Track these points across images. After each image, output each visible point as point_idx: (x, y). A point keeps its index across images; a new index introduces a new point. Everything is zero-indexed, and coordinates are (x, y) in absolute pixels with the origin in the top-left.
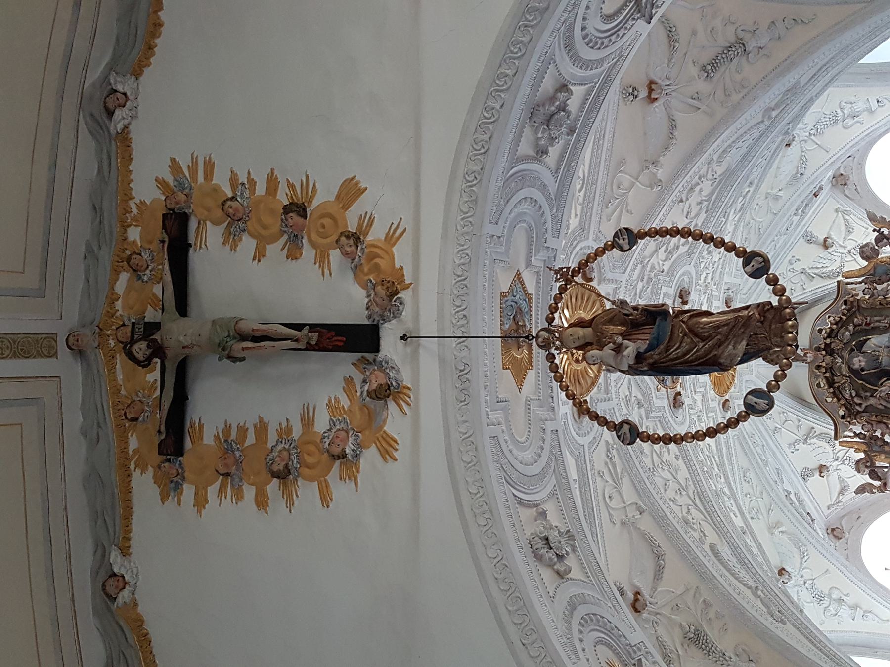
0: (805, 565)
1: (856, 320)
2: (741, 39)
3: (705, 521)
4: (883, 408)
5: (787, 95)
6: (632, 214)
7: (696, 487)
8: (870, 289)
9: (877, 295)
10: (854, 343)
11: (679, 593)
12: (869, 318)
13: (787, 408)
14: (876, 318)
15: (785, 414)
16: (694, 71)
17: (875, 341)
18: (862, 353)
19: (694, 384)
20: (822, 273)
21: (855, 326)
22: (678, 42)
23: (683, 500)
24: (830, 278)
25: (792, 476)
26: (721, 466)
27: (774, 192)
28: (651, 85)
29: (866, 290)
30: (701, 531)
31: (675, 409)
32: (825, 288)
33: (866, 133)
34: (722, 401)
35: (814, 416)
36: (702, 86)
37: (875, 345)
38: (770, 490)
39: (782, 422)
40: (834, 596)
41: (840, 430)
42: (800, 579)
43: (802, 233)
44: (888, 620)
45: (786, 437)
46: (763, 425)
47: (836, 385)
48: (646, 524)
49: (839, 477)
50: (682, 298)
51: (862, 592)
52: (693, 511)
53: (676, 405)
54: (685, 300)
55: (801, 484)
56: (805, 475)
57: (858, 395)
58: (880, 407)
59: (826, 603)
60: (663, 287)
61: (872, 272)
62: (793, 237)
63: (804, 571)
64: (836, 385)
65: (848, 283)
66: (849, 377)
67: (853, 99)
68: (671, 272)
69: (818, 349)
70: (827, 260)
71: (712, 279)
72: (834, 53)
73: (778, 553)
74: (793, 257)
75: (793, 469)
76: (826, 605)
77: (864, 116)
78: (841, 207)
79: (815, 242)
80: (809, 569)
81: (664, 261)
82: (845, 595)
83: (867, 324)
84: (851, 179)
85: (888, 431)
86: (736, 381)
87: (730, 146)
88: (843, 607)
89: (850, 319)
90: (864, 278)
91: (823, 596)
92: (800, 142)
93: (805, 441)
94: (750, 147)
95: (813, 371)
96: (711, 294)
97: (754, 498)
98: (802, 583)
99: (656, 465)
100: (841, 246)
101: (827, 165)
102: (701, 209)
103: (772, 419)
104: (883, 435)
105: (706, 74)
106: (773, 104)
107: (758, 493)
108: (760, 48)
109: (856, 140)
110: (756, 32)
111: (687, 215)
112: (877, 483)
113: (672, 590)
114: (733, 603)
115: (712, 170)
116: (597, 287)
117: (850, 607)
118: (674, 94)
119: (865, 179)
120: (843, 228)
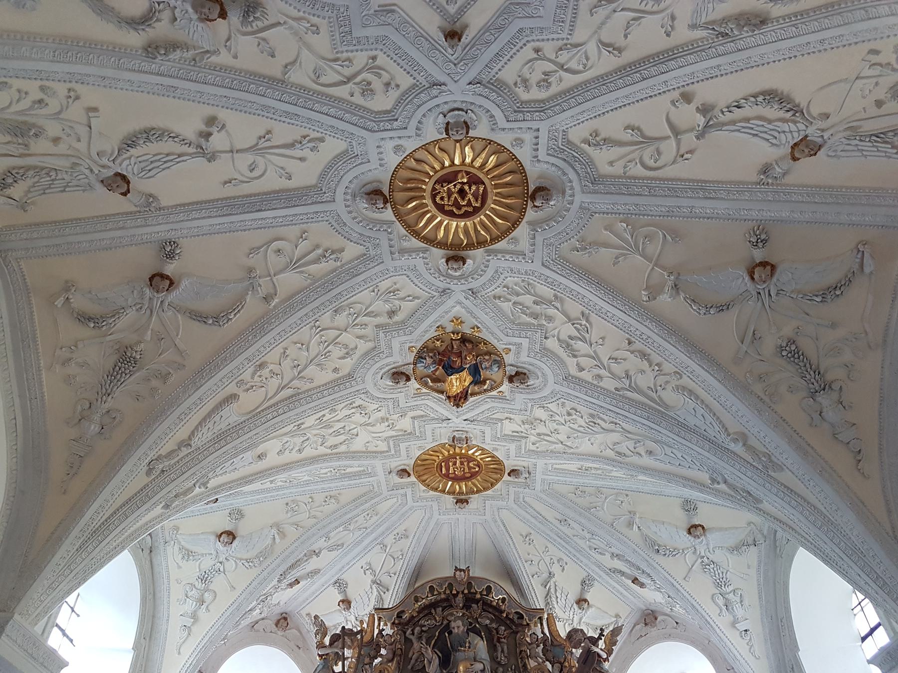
4: (410, 656)
5: (765, 457)
6: (614, 265)
8: (537, 641)
9: (530, 647)
10: (477, 625)
12: (505, 641)
13: (407, 559)
14: (505, 647)
16: (788, 331)
17: (481, 646)
19: (422, 416)
20: (550, 597)
24: (546, 605)
26: (334, 455)
27: (637, 520)
28: (769, 267)
29: (536, 637)
30: (253, 386)
31: (390, 375)
32: (535, 599)
36: (770, 343)
37: (476, 644)
38: (318, 526)
39: (393, 554)
40: (206, 595)
42: (224, 556)
43: (592, 574)
44: (179, 653)
45: (377, 558)
46: (387, 529)
47: (433, 611)
48: (253, 306)
50: (516, 374)
51: (211, 626)
52: (275, 382)
55: (330, 580)
56: (340, 584)
59: (199, 585)
61: (555, 643)
63: (233, 562)
64: (433, 611)
65: (541, 619)
66: (442, 623)
67: (746, 602)
69: (469, 585)
70: (564, 603)
71: (539, 434)
73: (252, 533)
74: (566, 564)
76: (196, 586)
77: (728, 618)
79: (583, 589)
80: (236, 568)
81: (559, 340)
82: (207, 607)
83: (499, 638)
84: (652, 629)
85: (385, 660)
86: (432, 493)
87: (697, 397)
90: (548, 635)
91: (207, 582)
92: (694, 546)
93: (374, 582)
94: (697, 429)
95: (446, 581)
97: (309, 508)
98: (221, 560)
100: (581, 619)
103: (394, 541)
106: (752, 441)
109: (700, 609)
112: (327, 641)
114: (168, 409)
115: (667, 382)
116: (525, 220)
117: (195, 611)
118: (760, 304)
119: (653, 644)
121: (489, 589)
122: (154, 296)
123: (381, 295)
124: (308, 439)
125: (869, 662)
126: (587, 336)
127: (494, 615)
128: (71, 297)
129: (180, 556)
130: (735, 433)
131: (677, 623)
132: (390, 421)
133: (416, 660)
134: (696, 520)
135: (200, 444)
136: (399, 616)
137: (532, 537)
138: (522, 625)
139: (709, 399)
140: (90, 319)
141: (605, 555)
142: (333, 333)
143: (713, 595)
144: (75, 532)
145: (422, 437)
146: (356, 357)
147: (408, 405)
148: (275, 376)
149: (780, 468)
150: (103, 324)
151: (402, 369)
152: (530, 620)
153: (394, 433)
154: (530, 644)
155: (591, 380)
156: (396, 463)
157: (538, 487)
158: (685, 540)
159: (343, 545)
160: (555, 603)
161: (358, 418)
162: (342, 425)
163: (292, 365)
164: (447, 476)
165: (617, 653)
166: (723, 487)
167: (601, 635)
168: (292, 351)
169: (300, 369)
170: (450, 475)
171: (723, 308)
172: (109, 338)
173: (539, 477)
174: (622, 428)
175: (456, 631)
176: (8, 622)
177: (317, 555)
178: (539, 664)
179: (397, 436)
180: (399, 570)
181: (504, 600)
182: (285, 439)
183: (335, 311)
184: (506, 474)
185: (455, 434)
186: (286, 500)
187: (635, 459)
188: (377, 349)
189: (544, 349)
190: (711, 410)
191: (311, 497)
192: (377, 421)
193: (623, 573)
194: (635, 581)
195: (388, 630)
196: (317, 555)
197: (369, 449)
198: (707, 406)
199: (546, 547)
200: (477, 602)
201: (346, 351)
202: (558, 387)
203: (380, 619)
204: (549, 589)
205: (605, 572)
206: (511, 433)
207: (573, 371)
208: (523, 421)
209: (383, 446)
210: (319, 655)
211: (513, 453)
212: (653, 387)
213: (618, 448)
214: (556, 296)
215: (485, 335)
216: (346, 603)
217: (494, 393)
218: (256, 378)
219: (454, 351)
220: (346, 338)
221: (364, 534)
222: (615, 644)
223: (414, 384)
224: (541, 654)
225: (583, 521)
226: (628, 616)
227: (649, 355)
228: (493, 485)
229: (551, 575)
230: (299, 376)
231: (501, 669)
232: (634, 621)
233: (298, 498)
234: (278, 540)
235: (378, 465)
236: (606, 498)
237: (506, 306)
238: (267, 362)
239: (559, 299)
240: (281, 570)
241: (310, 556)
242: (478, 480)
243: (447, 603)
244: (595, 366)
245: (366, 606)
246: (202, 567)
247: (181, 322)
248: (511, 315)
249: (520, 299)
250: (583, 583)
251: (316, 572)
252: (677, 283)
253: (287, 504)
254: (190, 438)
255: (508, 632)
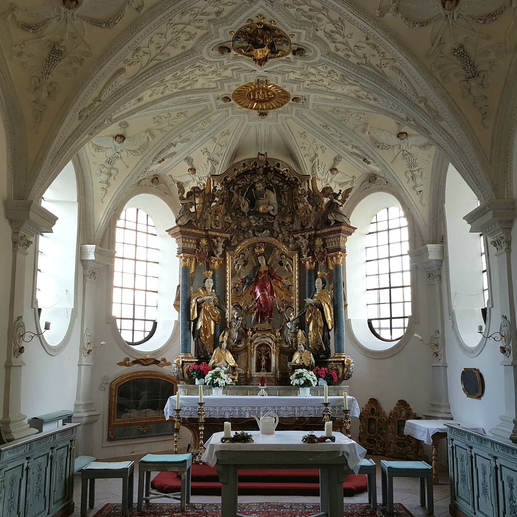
0: (129, 153)
1: (286, 186)
2: (478, 75)
3: (141, 67)
4: (232, 201)
5: (435, 113)
7: (164, 62)
9: (300, 197)
11: (85, 39)
12: (286, 193)
13: (229, 146)
14: (287, 197)
15: (225, 145)
18: (265, 189)
19: (238, 69)
20: (315, 168)
21: (282, 186)
22: (483, 23)
23: (154, 51)
24: (312, 172)
25: (186, 151)
26: (183, 91)
27: (368, 128)
30: (133, 62)
33: (401, 185)
34: (229, 96)
35: (226, 164)
36: (449, 47)
40: (112, 171)
41: (217, 178)
44: (102, 202)
45: (210, 145)
46: (217, 130)
47: (245, 176)
48: (129, 14)
49: (190, 181)
52: (146, 58)
53: (221, 49)
54: (296, 53)
55: (182, 157)
56: (189, 160)
57: (239, 188)
58: (232, 200)
59: (107, 165)
60: (305, 31)
61: (315, 194)
62: (339, 148)
63: (126, 153)
64: (245, 176)
65: (308, 181)
66: (250, 183)
67: (424, 176)
68: (316, 39)
69: (267, 163)
71: (311, 81)
72: (458, 142)
73: (134, 136)
74: (326, 149)
75: (191, 152)
77: (412, 184)
78: (356, 179)
81: (324, 31)
83: (283, 192)
84: (373, 185)
85: (218, 204)
86: (244, 109)
87: (403, 74)
88: (106, 176)
89: (285, 182)
90: (312, 190)
94: (401, 91)
96: (301, 81)
98: (118, 151)
99: (174, 27)
100: (332, 179)
101: (383, 162)
102: (360, 58)
104: (216, 201)
105: (457, 48)
106: (429, 103)
107: (172, 123)
108: (470, 89)
110: (481, 86)
111: (357, 47)
112: (185, 196)
113: (86, 33)
115: (387, 63)
118: (446, 22)
119: (372, 193)
120: (343, 181)
121: (278, 165)
122: (67, 11)
123: (211, 3)
124: (167, 87)
125: (464, 218)
126: (342, 32)
127: (281, 179)
128: (15, 14)
129: (94, 149)
130: (421, 97)
131: (387, 182)
132: (218, 73)
133: (236, 204)
134: (403, 129)
135: (105, 98)
136: (225, 179)
137: (306, 134)
138: (296, 184)
139: (409, 77)
140: (29, 27)
141: (348, 145)
142: (181, 27)
143: (406, 172)
144: (49, 155)
145: (239, 79)
146: (195, 40)
147: (229, 64)
148: (146, 55)
149: (442, 119)
150: (38, 30)
151: (226, 45)
152: (301, 182)
153: (220, 78)
154: (301, 195)
155: (343, 56)
156: (221, 94)
157: (310, 107)
158: (395, 140)
159: (189, 139)
160: (317, 171)
161: (197, 72)
162: (188, 76)
163: (156, 46)
164: (254, 100)
165: (347, 203)
166: (412, 122)
167: (340, 193)
168: (156, 39)
169: (161, 49)
170: (256, 99)
171: (423, 24)
172: (43, 39)
173: (311, 102)
174: (360, 84)
175: (258, 189)
176: (31, 205)
177: (175, 146)
178: (305, 206)
179: (222, 80)
180: (224, 152)
181: (287, 170)
182: (153, 89)
183: (182, 13)
184: (291, 100)
185: (259, 78)
186: (154, 116)
187: (367, 101)
188: (209, 34)
189: (315, 36)
190: (410, 83)
191: (169, 114)
192: (210, 73)
193: (358, 155)
194: (365, 160)
195: (219, 188)
196: (175, 146)
197: (205, 87)
198: (408, 80)
199: (314, 140)
200: (271, 171)
201: (189, 36)
202: (323, 58)
203: (214, 181)
204: (315, 163)
205: (348, 153)
206: (294, 79)
207: (333, 50)
208: (301, 73)
209: (213, 85)
210: (182, 204)
211: (295, 89)
212: (379, 64)
213: (358, 94)
214: (324, 8)
215: (278, 26)
216: (193, 170)
217: (284, 58)
218: (135, 57)
219: (259, 35)
220: (189, 28)
221: (202, 133)
222: (347, 197)
223: (233, 52)
224: (307, 201)
225: (336, 128)
226: (360, 177)
227: (378, 47)
228: (282, 105)
229: (316, 155)
230: (161, 52)
231: (283, 208)
232: (363, 180)
233: (161, 114)
234: (150, 139)
235: (211, 95)
236: (351, 115)
237: (292, 11)
238: (141, 47)
239: (325, 9)
240: (154, 156)
241: (171, 147)
242: (273, 102)
243: (254, 172)
244: (346, 49)
245: (205, 172)
246: (107, 155)
247: (86, 26)
248: (295, 16)
249: (301, 7)
250: (335, 159)
251: (174, 154)
252: (398, 7)
253: (154, 118)
254: (99, 96)
255: (288, 188)
